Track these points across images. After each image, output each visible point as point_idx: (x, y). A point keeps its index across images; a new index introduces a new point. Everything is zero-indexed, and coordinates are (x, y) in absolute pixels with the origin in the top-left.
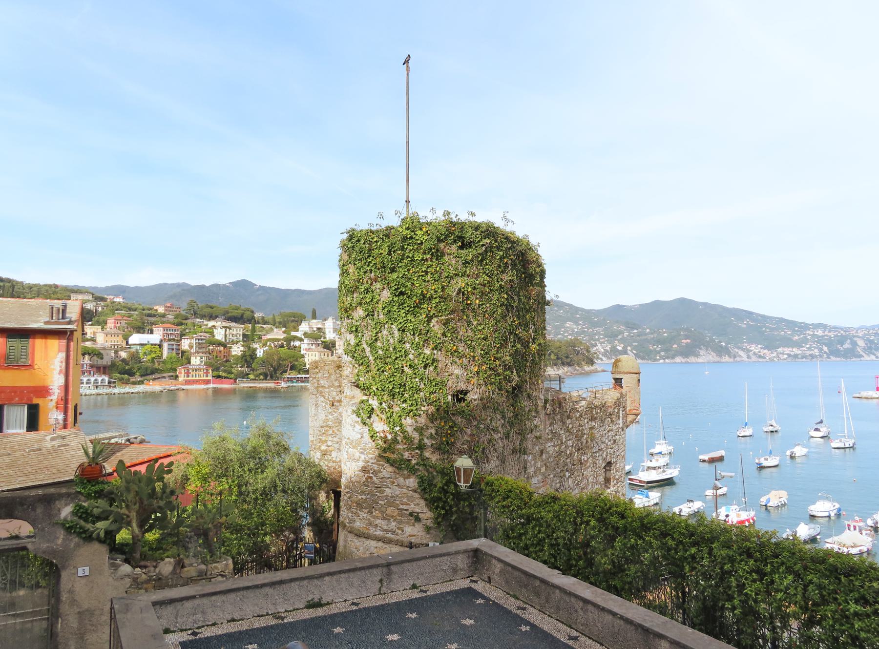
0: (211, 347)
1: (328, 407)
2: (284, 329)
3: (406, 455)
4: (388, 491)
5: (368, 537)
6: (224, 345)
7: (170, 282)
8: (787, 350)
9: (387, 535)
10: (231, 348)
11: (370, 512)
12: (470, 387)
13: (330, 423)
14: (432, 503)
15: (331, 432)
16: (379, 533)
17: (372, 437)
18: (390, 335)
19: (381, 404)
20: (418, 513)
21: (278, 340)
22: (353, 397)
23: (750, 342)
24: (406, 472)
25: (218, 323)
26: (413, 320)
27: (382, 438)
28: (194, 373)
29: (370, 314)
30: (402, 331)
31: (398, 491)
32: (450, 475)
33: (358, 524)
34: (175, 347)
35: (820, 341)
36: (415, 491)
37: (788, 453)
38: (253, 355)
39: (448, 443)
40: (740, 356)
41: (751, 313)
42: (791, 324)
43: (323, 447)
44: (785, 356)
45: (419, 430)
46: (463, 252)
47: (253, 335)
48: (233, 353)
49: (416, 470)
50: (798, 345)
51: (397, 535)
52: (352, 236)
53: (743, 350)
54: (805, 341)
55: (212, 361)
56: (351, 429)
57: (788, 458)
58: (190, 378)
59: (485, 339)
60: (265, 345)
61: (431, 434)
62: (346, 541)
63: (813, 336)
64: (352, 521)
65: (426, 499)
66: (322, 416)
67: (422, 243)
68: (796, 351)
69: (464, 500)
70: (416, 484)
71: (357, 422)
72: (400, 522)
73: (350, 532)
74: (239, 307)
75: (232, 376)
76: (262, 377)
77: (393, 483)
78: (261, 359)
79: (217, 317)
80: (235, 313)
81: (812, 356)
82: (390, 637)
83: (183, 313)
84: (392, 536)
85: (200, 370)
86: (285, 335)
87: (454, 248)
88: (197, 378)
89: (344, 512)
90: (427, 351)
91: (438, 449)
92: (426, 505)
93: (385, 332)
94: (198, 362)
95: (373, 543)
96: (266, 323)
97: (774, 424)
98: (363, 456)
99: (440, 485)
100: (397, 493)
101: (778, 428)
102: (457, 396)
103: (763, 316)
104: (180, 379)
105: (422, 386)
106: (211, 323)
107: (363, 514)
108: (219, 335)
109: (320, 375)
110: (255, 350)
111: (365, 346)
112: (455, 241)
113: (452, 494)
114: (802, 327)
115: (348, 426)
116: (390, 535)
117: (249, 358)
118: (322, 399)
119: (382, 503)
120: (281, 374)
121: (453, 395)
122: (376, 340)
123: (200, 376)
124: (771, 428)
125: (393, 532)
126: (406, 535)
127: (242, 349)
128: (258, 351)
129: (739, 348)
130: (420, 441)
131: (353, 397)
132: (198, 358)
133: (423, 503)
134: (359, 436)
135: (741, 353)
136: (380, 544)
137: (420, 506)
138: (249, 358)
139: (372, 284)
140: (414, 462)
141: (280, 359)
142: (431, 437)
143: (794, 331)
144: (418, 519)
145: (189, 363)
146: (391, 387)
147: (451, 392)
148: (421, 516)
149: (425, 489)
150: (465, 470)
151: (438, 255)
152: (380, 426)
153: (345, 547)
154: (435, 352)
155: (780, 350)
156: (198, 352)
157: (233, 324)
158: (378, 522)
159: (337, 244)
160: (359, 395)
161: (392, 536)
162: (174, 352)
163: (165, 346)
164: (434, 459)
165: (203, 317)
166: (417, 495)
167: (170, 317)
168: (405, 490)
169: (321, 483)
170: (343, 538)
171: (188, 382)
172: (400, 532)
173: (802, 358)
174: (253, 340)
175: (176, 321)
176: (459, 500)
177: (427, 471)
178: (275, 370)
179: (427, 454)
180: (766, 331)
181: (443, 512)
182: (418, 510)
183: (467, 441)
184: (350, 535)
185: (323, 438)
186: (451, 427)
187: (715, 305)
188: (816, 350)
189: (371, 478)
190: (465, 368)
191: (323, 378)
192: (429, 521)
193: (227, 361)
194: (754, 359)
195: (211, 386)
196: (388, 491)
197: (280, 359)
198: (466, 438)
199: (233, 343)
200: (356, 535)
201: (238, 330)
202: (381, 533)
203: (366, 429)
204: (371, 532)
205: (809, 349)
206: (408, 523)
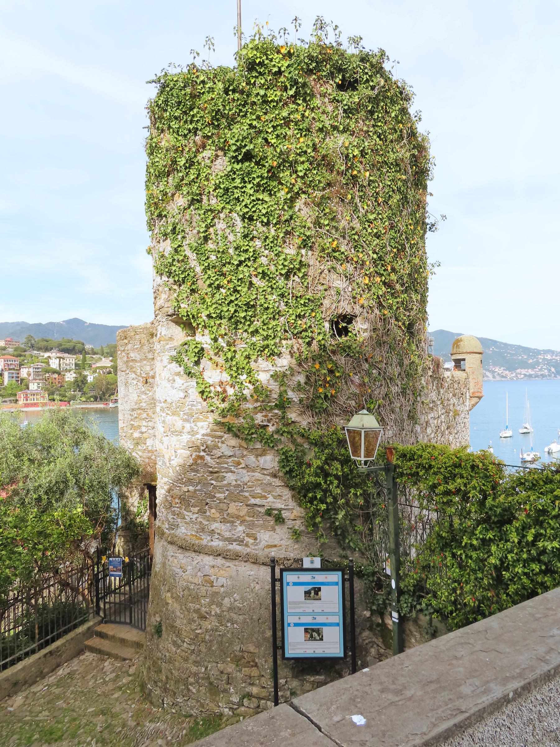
0: (47, 375)
1: (140, 384)
2: (111, 358)
3: (259, 418)
4: (230, 478)
5: (198, 550)
6: (59, 373)
7: (10, 321)
8: (524, 371)
9: (230, 547)
10: (64, 375)
11: (202, 512)
12: (358, 310)
13: (144, 405)
14: (303, 493)
15: (144, 415)
16: (217, 544)
17: (202, 393)
18: (229, 230)
19: (215, 340)
20: (280, 510)
21: (106, 368)
22: (171, 339)
23: (495, 365)
24: (258, 446)
25: (53, 354)
26: (267, 199)
27: (218, 394)
28: (32, 397)
29: (195, 201)
30: (249, 218)
31: (246, 476)
32: (338, 448)
33: (183, 531)
34: (14, 375)
35: (549, 363)
36: (275, 476)
37: (546, 450)
38: (84, 381)
39: (326, 396)
40: (487, 376)
41: (496, 342)
42: (526, 350)
43: (136, 435)
44: (522, 376)
45: (280, 378)
46: (345, 96)
47: (84, 364)
48: (67, 380)
49: (276, 442)
50: (532, 367)
51: (247, 545)
52: (165, 86)
53: (489, 371)
54: (538, 363)
55: (48, 386)
56: (169, 385)
57: (547, 453)
58: (28, 402)
59: (377, 236)
60: (94, 372)
61: (299, 384)
62: (164, 556)
63: (544, 359)
64: (173, 526)
65: (292, 488)
66: (134, 397)
67: (280, 73)
68: (530, 372)
69: (356, 486)
70: (276, 465)
71: (178, 374)
72: (251, 525)
73: (171, 543)
74: (73, 341)
75: (66, 399)
76: (92, 399)
77: (239, 463)
78: (91, 383)
79: (52, 349)
80: (68, 345)
81: (543, 376)
83: (23, 346)
84: (238, 548)
85: (37, 394)
86: (112, 363)
87: (330, 88)
88: (35, 401)
89: (161, 511)
90: (290, 251)
91: (309, 407)
92: (293, 496)
93: (220, 225)
94: (36, 388)
95: (208, 560)
96: (95, 353)
97: (528, 427)
98: (188, 426)
99: (317, 463)
100: (246, 479)
101: (531, 430)
102: (337, 323)
103: (506, 344)
104: (21, 402)
105: (283, 307)
106: (46, 355)
107: (191, 515)
108: (54, 364)
109: (130, 346)
110: (86, 376)
111: (188, 253)
112: (331, 75)
113: (337, 477)
114: (534, 352)
115: (165, 383)
116: (235, 547)
117: (80, 384)
118: (133, 376)
119: (221, 496)
120: (110, 396)
121: (331, 322)
122: (206, 239)
123: (37, 399)
124: (525, 430)
125: (240, 542)
126: (261, 546)
127: (74, 375)
128: (89, 377)
129: (486, 370)
130: (280, 395)
131: (171, 339)
132: (36, 384)
133: (287, 493)
134: (182, 395)
135: (488, 374)
136: (220, 561)
137: (282, 499)
138: (80, 384)
139: (198, 151)
140: (271, 429)
141: (108, 383)
142: (299, 388)
143: (529, 355)
144: (280, 520)
145: (28, 388)
146: (232, 310)
147: (329, 315)
148: (285, 514)
149: (291, 471)
150: (366, 433)
151: (302, 94)
152: (214, 375)
153: (164, 564)
154: (303, 251)
155: (518, 371)
156: (36, 379)
157: (66, 355)
158: (215, 526)
159: (145, 103)
160: (179, 334)
161: (238, 548)
162: (14, 379)
163: (6, 374)
164: (304, 424)
165: (39, 349)
166: (277, 482)
167: (10, 350)
168: (257, 475)
169: (131, 475)
170: (158, 548)
171: (27, 405)
172: (251, 541)
173: (535, 377)
174: (84, 368)
175: (15, 353)
176: (348, 487)
177: (294, 441)
178: (104, 394)
179: (292, 416)
180: (507, 356)
181: (323, 507)
182: (279, 506)
183: (355, 395)
184: (171, 548)
185: (136, 424)
186: (331, 372)
188: (546, 371)
189: (202, 458)
190: (349, 278)
191: (133, 350)
192: (298, 522)
193: (61, 386)
194: (498, 378)
195: (46, 408)
196: (230, 478)
197: (108, 383)
198: (354, 389)
199: (66, 370)
200: (181, 547)
201: (71, 360)
202: (221, 543)
203: (193, 382)
204: (204, 542)
205: (541, 370)
206: (264, 527)
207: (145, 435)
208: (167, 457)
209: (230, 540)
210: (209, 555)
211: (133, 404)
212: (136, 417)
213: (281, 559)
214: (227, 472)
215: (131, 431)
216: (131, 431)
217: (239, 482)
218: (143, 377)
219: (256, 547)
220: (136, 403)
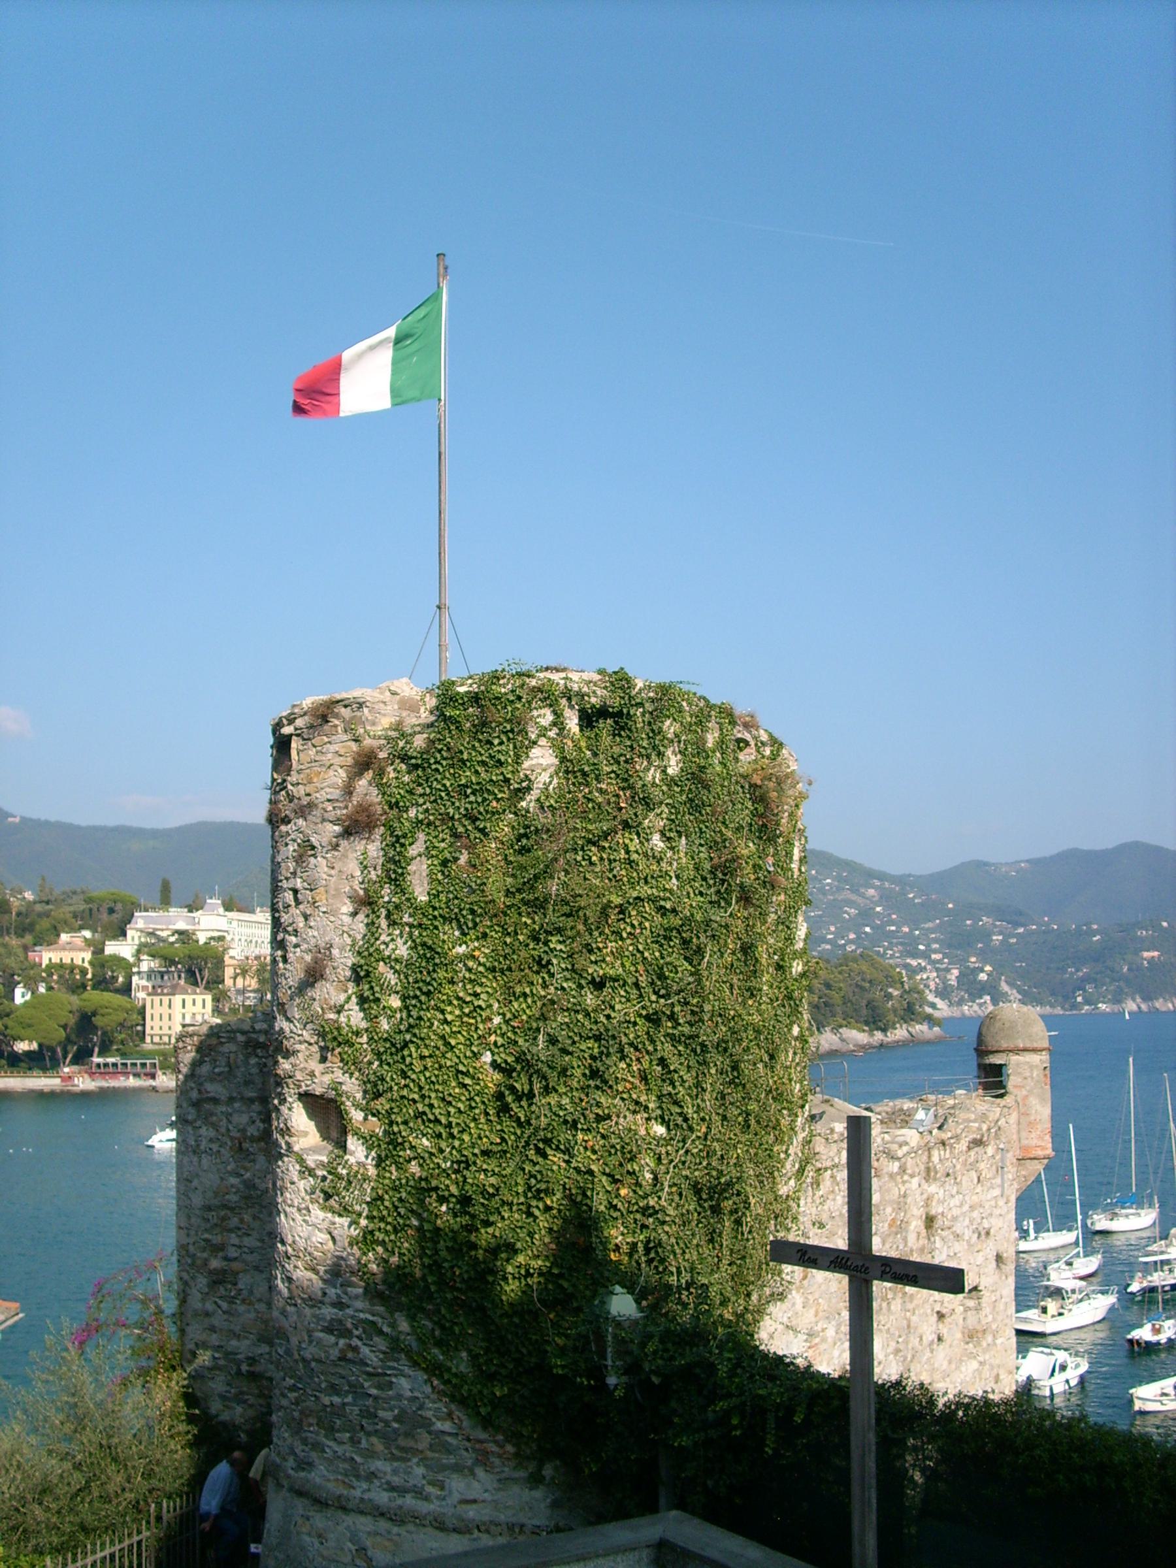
5: (342, 1506)
11: (354, 1442)
15: (235, 1221)
16: (382, 1498)
43: (215, 1264)
51: (427, 1499)
73: (300, 1493)
82: (1098, 937)
95: (364, 1524)
116: (409, 1501)
118: (212, 1133)
125: (419, 1493)
136: (383, 1525)
158: (378, 1464)
184: (300, 1505)
187: (1102, 851)
207: (235, 1266)
208: (294, 1340)
209: (402, 1491)
210: (366, 1514)
211: (210, 1194)
212: (216, 1225)
213: (484, 1524)
214: (396, 1376)
215: (205, 1255)
216: (205, 1255)
217: (417, 1394)
218: (232, 1138)
219: (444, 1503)
220: (216, 1194)
